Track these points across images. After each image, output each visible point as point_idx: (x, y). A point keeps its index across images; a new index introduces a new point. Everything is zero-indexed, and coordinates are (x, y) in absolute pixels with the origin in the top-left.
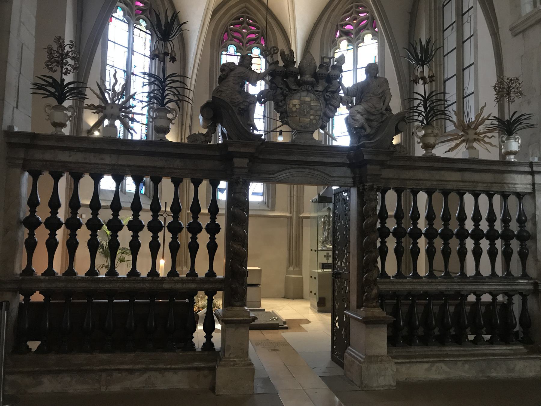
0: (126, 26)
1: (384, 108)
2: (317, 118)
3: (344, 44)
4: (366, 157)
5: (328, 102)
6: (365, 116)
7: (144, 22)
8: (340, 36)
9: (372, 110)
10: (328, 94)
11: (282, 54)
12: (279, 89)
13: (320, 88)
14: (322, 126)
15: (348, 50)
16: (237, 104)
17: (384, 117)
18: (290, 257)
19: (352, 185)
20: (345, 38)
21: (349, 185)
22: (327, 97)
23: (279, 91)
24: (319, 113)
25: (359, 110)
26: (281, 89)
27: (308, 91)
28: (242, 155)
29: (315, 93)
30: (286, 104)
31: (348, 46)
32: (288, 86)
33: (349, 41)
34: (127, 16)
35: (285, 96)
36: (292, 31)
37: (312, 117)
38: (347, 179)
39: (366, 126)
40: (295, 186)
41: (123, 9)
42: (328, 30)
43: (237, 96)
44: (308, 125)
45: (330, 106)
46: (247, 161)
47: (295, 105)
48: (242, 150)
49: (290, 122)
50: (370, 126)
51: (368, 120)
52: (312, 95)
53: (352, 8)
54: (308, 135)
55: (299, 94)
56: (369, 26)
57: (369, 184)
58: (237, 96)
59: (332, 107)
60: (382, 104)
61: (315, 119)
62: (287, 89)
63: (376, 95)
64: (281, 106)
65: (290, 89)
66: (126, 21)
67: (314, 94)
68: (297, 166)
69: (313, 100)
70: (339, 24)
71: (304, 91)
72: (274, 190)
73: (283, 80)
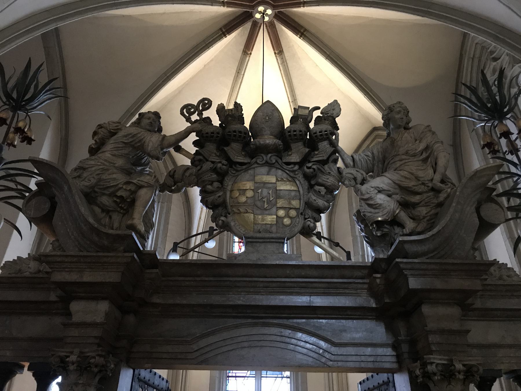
1: (438, 177)
2: (293, 213)
4: (414, 283)
5: (313, 182)
6: (397, 197)
9: (410, 184)
10: (310, 165)
11: (221, 110)
12: (209, 163)
13: (295, 158)
14: (303, 228)
16: (111, 190)
17: (442, 196)
19: (395, 366)
21: (387, 366)
22: (308, 171)
23: (207, 166)
24: (295, 203)
25: (381, 185)
26: (213, 162)
27: (269, 165)
28: (92, 292)
29: (285, 167)
30: (222, 187)
32: (229, 159)
35: (222, 176)
37: (281, 213)
38: (380, 351)
39: (403, 216)
40: (334, 374)
43: (114, 176)
44: (274, 229)
45: (317, 188)
46: (103, 306)
47: (243, 192)
48: (88, 277)
49: (232, 224)
50: (413, 219)
51: (404, 205)
52: (280, 172)
54: (271, 247)
55: (251, 172)
57: (437, 360)
58: (114, 176)
59: (322, 188)
60: (431, 171)
61: (287, 216)
62: (224, 162)
63: (414, 155)
64: (212, 192)
65: (231, 163)
68: (250, 320)
69: (282, 180)
71: (262, 165)
72: (305, 382)
73: (218, 149)
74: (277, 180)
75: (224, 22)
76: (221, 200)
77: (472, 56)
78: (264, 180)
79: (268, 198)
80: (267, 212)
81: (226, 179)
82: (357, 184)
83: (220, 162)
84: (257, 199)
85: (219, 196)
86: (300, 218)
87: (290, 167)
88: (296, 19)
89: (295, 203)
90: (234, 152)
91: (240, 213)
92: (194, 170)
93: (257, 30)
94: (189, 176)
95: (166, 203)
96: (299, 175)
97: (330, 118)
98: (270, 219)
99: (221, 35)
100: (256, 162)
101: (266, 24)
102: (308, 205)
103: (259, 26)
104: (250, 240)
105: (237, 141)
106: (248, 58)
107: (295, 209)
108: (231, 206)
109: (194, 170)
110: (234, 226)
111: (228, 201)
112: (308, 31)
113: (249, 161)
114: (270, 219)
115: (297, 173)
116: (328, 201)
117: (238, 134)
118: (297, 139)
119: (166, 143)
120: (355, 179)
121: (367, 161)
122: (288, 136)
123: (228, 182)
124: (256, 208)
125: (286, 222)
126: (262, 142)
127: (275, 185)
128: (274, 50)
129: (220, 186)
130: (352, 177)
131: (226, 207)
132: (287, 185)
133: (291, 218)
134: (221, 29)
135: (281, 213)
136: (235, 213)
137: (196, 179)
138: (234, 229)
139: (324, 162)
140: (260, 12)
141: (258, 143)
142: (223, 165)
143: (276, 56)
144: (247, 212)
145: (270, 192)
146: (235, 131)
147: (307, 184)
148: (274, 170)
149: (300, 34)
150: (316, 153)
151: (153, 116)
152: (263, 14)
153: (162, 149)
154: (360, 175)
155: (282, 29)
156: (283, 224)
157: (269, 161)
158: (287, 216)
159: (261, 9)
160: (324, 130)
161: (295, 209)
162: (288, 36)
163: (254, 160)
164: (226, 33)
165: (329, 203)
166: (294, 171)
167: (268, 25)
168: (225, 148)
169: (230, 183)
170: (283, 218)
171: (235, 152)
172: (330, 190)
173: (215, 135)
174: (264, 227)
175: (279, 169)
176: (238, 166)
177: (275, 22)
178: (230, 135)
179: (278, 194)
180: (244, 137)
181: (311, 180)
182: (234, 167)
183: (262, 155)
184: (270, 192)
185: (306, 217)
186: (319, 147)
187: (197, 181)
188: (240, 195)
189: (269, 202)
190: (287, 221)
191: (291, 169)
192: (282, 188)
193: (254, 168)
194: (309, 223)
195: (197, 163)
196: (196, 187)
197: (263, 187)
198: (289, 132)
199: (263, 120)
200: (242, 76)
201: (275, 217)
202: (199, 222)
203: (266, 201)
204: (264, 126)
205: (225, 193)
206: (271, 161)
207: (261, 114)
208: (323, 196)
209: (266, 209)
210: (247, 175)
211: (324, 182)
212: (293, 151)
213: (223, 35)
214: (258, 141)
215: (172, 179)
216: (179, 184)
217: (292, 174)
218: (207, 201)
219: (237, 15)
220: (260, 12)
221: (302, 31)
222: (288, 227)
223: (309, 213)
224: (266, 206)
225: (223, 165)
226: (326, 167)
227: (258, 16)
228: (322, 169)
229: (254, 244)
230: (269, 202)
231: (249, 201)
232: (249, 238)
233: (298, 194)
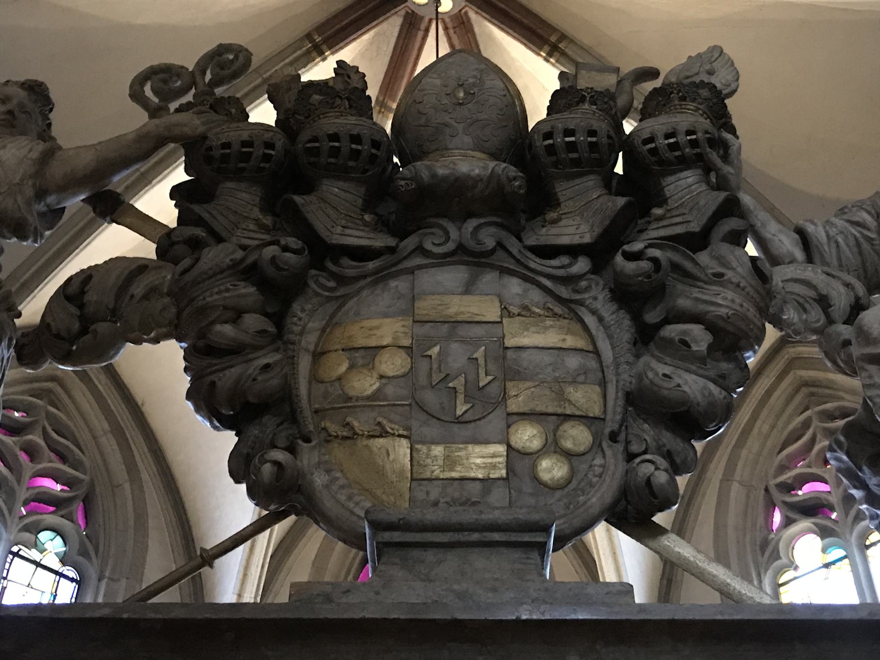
2: (577, 437)
7: (59, 539)
8: (788, 522)
13: (573, 228)
14: (625, 492)
15: (827, 566)
20: (805, 523)
24: (584, 397)
27: (474, 258)
29: (535, 263)
30: (279, 333)
31: (824, 550)
33: (824, 532)
35: (278, 294)
37: (527, 436)
42: (732, 519)
45: (672, 331)
49: (319, 479)
52: (514, 287)
53: (806, 425)
55: (400, 284)
59: (696, 329)
61: (553, 446)
62: (293, 242)
64: (235, 351)
65: (321, 252)
67: (529, 278)
70: (772, 483)
71: (445, 260)
73: (269, 205)
74: (505, 311)
76: (273, 381)
78: (452, 311)
79: (471, 378)
80: (467, 431)
81: (296, 307)
82: (830, 321)
83: (276, 243)
84: (423, 380)
85: (267, 366)
86: (608, 452)
87: (555, 262)
89: (584, 397)
90: (330, 211)
91: (353, 436)
92: (168, 275)
94: (146, 297)
95: (124, 582)
96: (593, 293)
97: (705, 93)
98: (482, 459)
99: (308, 52)
100: (420, 250)
101: (444, 21)
102: (642, 402)
103: (423, 26)
104: (396, 536)
105: (341, 173)
107: (584, 419)
108: (316, 412)
109: (168, 275)
110: (327, 487)
111: (303, 390)
112: (572, 41)
113: (391, 242)
114: (482, 459)
115: (584, 284)
116: (720, 380)
117: (345, 146)
118: (576, 163)
119: (57, 170)
120: (824, 302)
121: (858, 244)
122: (542, 152)
123: (307, 320)
124: (423, 416)
125: (549, 470)
126: (441, 172)
127: (497, 330)
129: (272, 329)
130: (812, 293)
131: (293, 417)
132: (546, 328)
133: (568, 455)
134: (309, 36)
135: (527, 436)
136: (329, 438)
137: (174, 310)
138: (328, 504)
139: (696, 242)
141: (425, 175)
142: (286, 249)
144: (384, 434)
145: (479, 354)
146: (334, 137)
147: (627, 322)
148: (489, 278)
149: (547, 48)
150: (657, 211)
151: (22, 94)
153: (41, 194)
154: (842, 289)
155: (491, 37)
156: (536, 479)
157: (471, 244)
158: (553, 446)
160: (683, 127)
161: (584, 419)
163: (410, 242)
164: (324, 47)
165: (729, 390)
166: (568, 280)
167: (450, 25)
168: (298, 199)
169: (315, 325)
170: (533, 456)
171: (336, 212)
172: (729, 341)
173: (259, 151)
174: (454, 492)
175: (512, 273)
176: (346, 261)
177: (473, 15)
178: (316, 152)
179: (508, 365)
180: (373, 158)
181: (643, 306)
182: (330, 265)
183: (444, 222)
184: (479, 354)
185: (635, 448)
186: (668, 191)
187: (179, 315)
188: (351, 367)
189: (474, 392)
190: (552, 469)
191: (561, 273)
192: (525, 341)
193: (411, 271)
194: (649, 468)
195: (180, 249)
196: (173, 342)
197: (450, 336)
198: (548, 135)
199: (445, 101)
201: (501, 449)
203: (461, 389)
204: (447, 118)
205: (292, 361)
206: (479, 243)
207: (438, 82)
208: (702, 360)
209: (459, 421)
210: (384, 297)
211: (702, 307)
212: (564, 209)
213: (314, 54)
214: (429, 168)
215: (73, 310)
216: (102, 327)
217: (564, 292)
218: (213, 384)
221: (553, 39)
222: (558, 494)
223: (646, 432)
224: (461, 409)
225: (286, 249)
226: (703, 257)
228: (688, 265)
229: (415, 553)
230: (474, 392)
231: (390, 390)
232: (391, 527)
233: (593, 364)
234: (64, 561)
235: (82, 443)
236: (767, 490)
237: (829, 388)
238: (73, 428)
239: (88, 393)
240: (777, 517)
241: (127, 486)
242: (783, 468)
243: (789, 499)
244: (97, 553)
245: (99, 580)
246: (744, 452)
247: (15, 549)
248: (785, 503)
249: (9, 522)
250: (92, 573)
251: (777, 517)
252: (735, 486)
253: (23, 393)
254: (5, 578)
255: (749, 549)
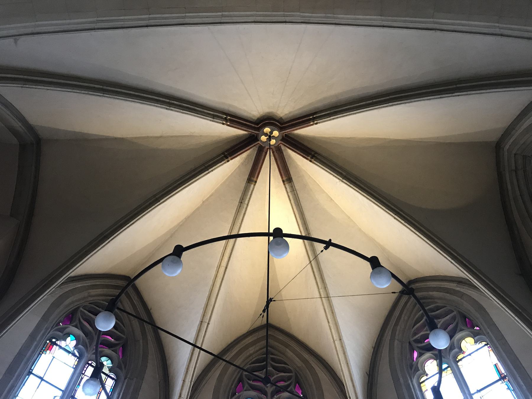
0: (72, 361)
3: (431, 366)
7: (109, 361)
8: (420, 355)
18: (321, 111)
20: (428, 354)
34: (80, 346)
36: (343, 377)
41: (77, 338)
42: (396, 351)
56: (460, 326)
66: (77, 354)
70: (412, 339)
75: (228, 147)
77: (514, 168)
88: (306, 144)
93: (263, 157)
95: (135, 379)
106: (252, 186)
128: (282, 178)
134: (223, 153)
140: (266, 135)
143: (284, 184)
152: (270, 136)
155: (289, 156)
159: (267, 130)
162: (297, 160)
167: (274, 150)
177: (283, 148)
200: (245, 206)
202: (182, 390)
213: (224, 158)
219: (241, 140)
220: (266, 135)
227: (264, 138)
234: (110, 371)
235: (124, 322)
236: (410, 343)
237: (429, 299)
238: (122, 316)
239: (129, 303)
240: (416, 355)
241: (141, 341)
242: (415, 334)
243: (420, 345)
244: (125, 368)
245: (125, 379)
246: (399, 327)
247: (90, 362)
248: (418, 347)
249: (89, 349)
250: (122, 375)
251: (416, 355)
252: (396, 342)
253: (103, 300)
254: (83, 374)
255: (405, 367)
